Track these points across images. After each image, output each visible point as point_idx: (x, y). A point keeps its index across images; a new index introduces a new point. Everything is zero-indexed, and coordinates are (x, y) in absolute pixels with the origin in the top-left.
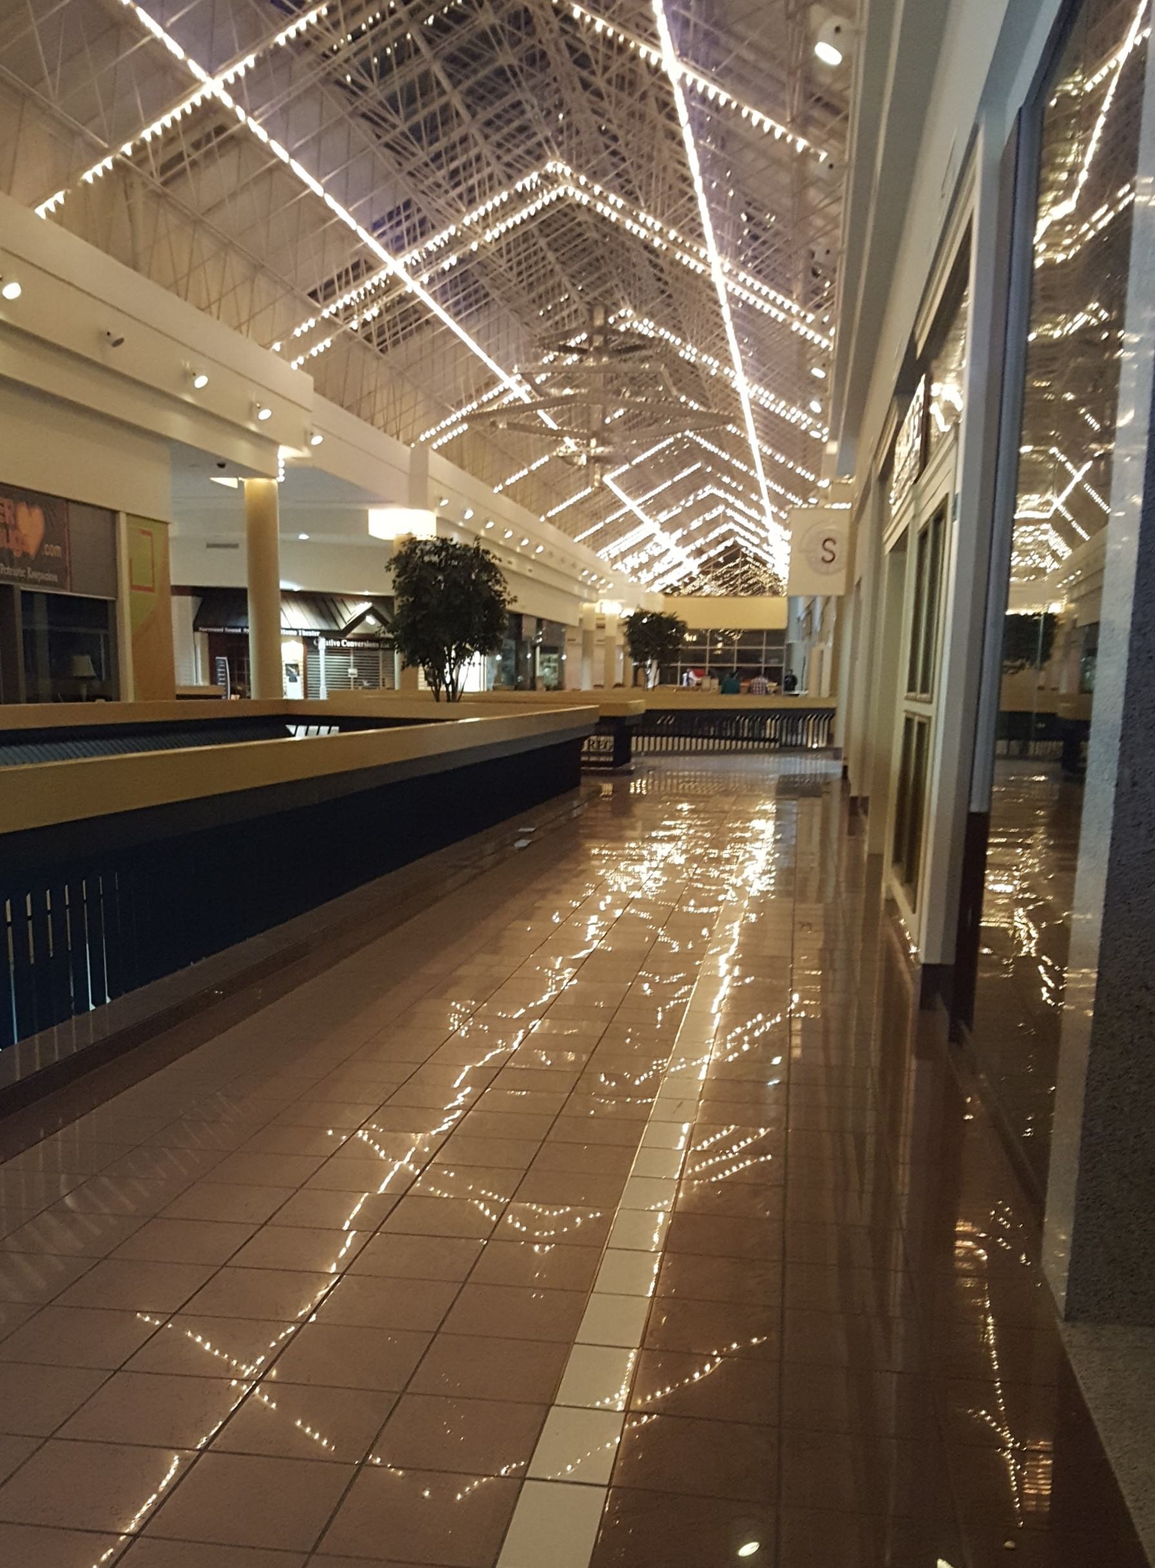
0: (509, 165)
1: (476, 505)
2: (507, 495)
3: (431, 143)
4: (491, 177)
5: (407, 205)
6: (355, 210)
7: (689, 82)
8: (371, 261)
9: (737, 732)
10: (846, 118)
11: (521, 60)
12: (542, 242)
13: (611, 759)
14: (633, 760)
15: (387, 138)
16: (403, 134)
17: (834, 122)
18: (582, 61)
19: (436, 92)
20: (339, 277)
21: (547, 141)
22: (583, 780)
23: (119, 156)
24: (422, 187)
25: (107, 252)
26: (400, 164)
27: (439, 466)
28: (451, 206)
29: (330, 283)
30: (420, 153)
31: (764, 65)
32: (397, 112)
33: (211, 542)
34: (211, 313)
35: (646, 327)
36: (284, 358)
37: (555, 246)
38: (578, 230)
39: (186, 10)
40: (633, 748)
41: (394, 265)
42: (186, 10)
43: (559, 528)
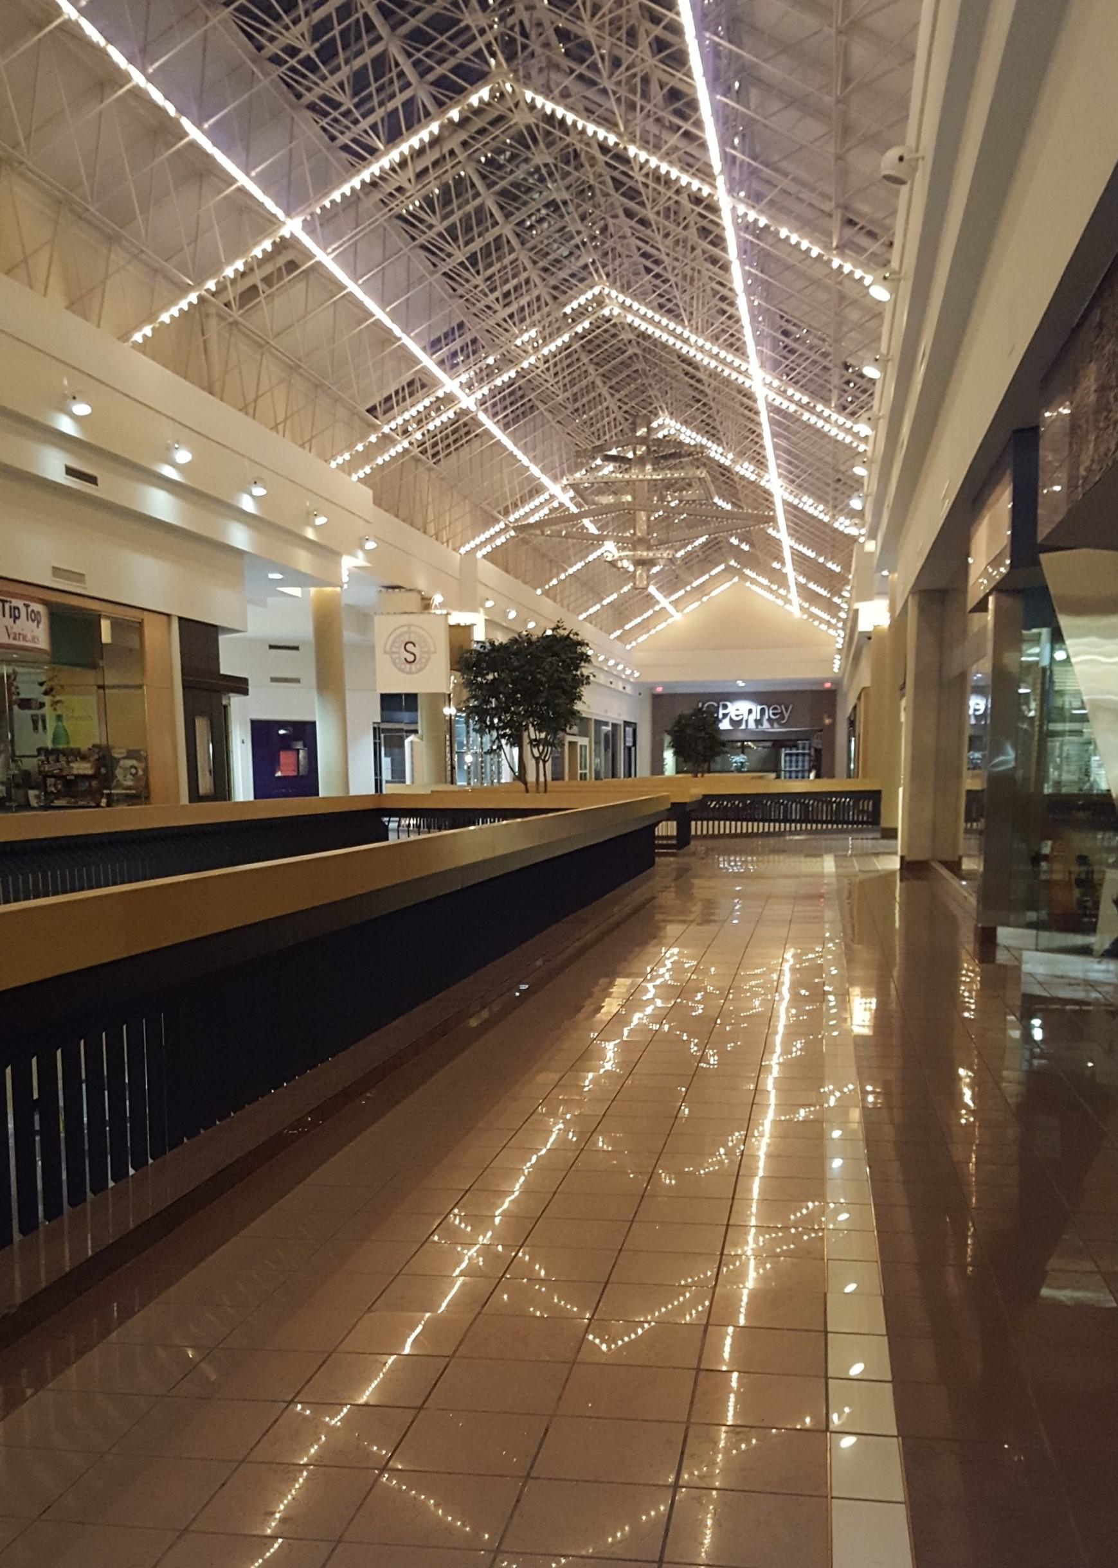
0: (555, 288)
1: (520, 607)
2: (591, 623)
3: (467, 244)
4: (538, 299)
5: (461, 325)
6: (258, 175)
7: (770, 399)
8: (425, 380)
9: (785, 815)
10: (872, 394)
11: (556, 158)
12: (585, 360)
13: (674, 842)
14: (693, 843)
15: (422, 240)
16: (440, 235)
17: (875, 247)
18: (632, 194)
19: (470, 193)
20: (397, 393)
21: (584, 244)
22: (657, 859)
23: (203, 293)
24: (474, 310)
25: (185, 378)
26: (435, 265)
27: (489, 572)
28: (499, 325)
29: (388, 398)
30: (456, 252)
31: (805, 195)
32: (434, 212)
33: (273, 643)
34: (247, 414)
35: (689, 436)
36: (344, 471)
37: (589, 347)
38: (613, 331)
39: (171, 54)
40: (693, 833)
41: (449, 384)
42: (171, 54)
43: (596, 625)
